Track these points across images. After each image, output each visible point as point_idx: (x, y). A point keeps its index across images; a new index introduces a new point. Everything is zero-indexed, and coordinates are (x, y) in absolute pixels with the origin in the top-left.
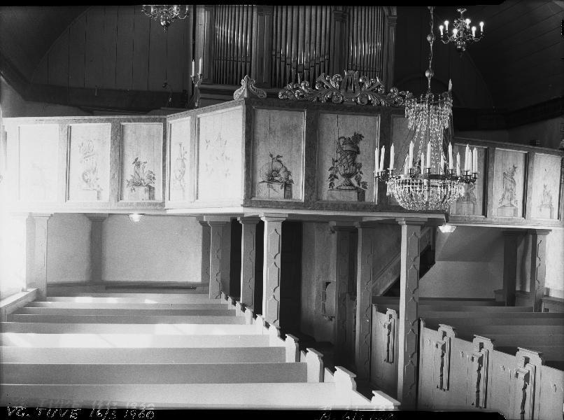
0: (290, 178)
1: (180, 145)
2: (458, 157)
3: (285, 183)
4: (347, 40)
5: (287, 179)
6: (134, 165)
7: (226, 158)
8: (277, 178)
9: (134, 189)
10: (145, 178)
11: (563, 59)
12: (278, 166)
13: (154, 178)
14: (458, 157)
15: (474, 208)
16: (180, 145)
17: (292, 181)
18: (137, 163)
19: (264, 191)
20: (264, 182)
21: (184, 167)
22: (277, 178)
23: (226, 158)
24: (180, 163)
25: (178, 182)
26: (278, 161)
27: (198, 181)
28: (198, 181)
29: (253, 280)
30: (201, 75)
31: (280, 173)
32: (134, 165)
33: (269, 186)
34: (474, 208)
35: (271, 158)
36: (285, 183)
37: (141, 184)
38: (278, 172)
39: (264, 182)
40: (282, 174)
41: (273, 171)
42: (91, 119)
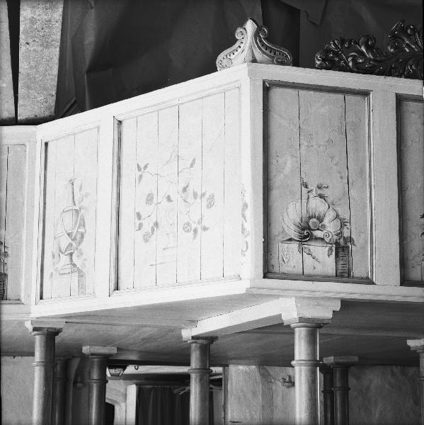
0: (346, 234)
3: (337, 243)
4: (368, 161)
5: (340, 234)
7: (195, 195)
8: (318, 234)
11: (271, 423)
12: (317, 205)
17: (350, 239)
19: (289, 257)
22: (318, 234)
24: (69, 220)
26: (321, 196)
27: (45, 176)
28: (45, 176)
29: (270, 204)
31: (326, 222)
33: (301, 251)
36: (337, 243)
38: (320, 219)
40: (331, 227)
41: (310, 218)
42: (26, 270)
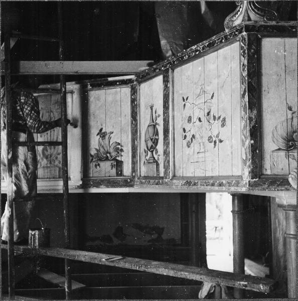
1: (151, 108)
2: (110, 79)
6: (99, 136)
7: (214, 117)
9: (99, 165)
10: (111, 150)
13: (122, 150)
14: (110, 79)
15: (150, 163)
16: (151, 108)
18: (102, 135)
20: (279, 149)
21: (157, 134)
23: (214, 117)
25: (149, 153)
30: (258, 11)
32: (99, 136)
34: (150, 163)
35: (290, 113)
37: (107, 159)
39: (279, 149)
